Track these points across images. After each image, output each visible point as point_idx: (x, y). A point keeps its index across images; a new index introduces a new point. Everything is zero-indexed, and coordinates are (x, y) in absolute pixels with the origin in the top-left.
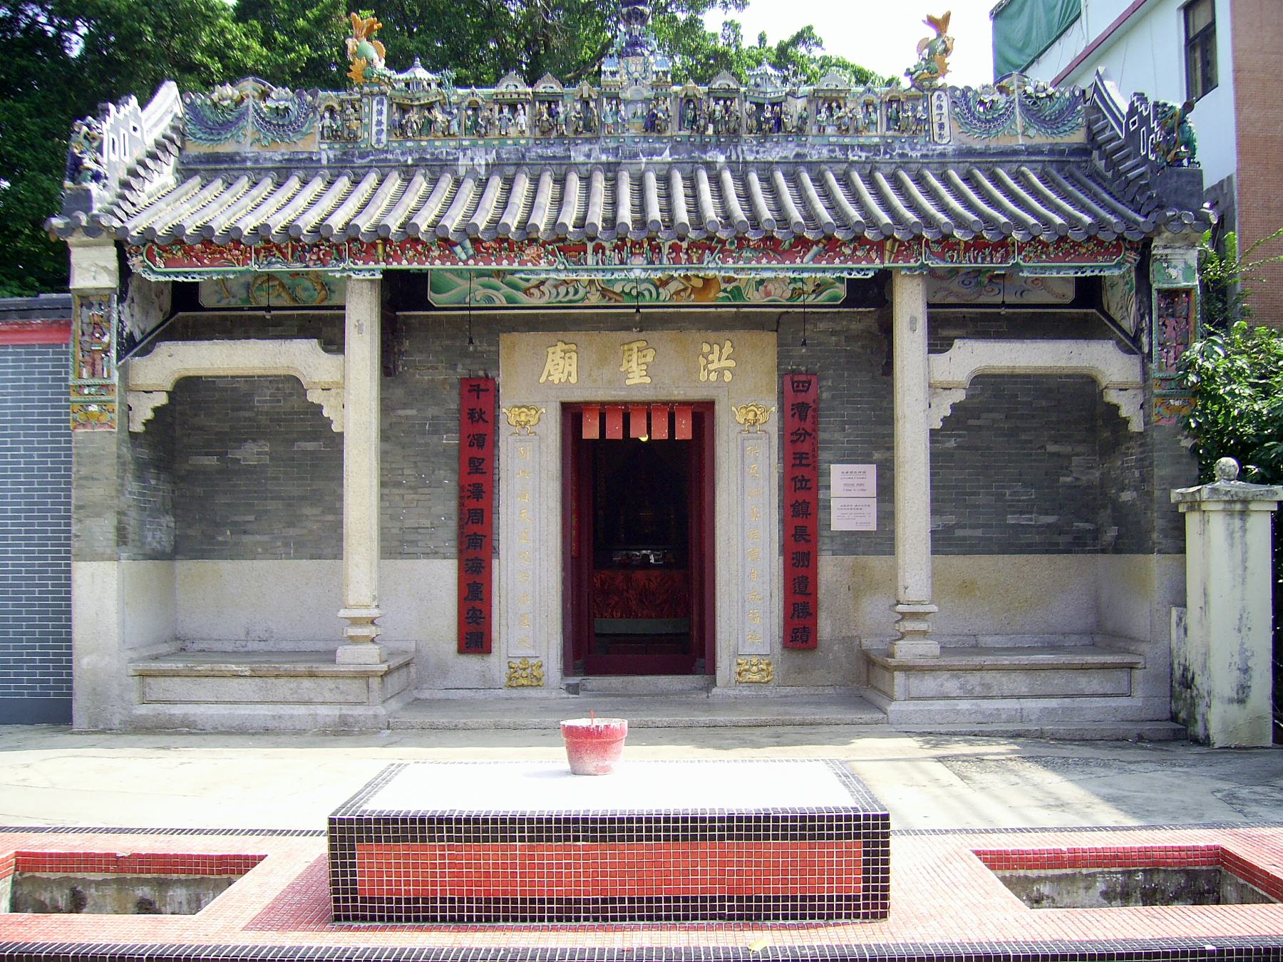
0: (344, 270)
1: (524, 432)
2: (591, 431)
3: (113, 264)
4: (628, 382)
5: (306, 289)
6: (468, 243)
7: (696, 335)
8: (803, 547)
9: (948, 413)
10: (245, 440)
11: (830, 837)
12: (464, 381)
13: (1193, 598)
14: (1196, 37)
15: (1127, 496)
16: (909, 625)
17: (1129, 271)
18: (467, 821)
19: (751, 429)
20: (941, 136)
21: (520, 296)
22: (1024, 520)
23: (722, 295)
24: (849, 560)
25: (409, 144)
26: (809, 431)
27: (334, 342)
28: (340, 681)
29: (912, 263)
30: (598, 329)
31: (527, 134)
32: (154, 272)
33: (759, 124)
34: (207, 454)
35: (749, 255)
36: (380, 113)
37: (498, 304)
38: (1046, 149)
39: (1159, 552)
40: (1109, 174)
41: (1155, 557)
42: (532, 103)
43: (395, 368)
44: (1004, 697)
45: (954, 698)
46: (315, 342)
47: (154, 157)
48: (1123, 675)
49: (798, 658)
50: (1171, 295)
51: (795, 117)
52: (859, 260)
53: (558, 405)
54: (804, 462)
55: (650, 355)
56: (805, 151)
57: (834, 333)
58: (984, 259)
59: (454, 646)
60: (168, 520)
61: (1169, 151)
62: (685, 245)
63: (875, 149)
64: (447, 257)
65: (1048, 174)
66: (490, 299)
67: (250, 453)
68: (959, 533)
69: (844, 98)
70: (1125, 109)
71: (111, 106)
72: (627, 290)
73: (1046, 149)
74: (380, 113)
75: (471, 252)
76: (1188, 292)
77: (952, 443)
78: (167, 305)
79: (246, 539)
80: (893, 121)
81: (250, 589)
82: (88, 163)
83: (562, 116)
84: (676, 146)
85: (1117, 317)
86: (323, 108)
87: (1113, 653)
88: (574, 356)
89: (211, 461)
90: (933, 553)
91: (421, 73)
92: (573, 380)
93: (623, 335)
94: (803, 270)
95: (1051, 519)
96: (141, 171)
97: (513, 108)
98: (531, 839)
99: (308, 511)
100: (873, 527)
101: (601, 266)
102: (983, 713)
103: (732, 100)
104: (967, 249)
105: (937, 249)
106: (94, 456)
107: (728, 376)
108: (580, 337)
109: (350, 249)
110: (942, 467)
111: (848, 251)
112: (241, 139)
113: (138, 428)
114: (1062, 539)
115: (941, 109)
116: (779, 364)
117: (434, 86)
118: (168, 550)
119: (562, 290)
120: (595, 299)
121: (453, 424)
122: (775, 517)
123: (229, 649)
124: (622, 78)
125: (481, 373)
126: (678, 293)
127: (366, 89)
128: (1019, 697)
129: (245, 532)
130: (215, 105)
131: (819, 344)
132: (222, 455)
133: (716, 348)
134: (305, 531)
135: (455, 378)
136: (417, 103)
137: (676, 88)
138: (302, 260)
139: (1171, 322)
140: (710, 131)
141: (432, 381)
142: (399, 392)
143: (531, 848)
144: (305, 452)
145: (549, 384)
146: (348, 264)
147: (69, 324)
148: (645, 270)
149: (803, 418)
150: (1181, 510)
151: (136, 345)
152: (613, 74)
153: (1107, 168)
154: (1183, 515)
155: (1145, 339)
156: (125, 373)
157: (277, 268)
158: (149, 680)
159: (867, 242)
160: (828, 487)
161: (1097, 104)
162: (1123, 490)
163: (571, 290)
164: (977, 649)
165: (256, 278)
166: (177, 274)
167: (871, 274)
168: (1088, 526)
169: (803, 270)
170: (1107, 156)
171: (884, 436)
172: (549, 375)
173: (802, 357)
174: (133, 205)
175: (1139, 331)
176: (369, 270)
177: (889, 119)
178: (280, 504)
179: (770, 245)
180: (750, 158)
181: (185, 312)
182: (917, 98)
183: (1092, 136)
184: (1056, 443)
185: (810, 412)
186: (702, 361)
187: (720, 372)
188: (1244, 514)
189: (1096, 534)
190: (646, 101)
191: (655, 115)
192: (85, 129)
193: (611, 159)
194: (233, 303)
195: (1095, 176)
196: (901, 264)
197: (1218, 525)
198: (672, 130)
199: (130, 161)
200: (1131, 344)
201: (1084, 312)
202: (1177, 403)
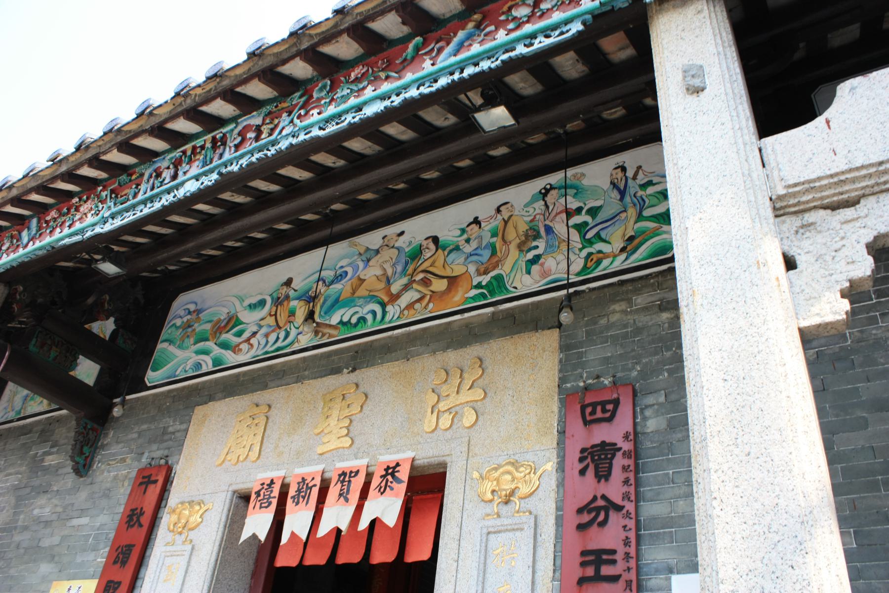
37: (205, 369)
54: (606, 570)
72: (345, 319)
116: (562, 381)
126: (410, 306)
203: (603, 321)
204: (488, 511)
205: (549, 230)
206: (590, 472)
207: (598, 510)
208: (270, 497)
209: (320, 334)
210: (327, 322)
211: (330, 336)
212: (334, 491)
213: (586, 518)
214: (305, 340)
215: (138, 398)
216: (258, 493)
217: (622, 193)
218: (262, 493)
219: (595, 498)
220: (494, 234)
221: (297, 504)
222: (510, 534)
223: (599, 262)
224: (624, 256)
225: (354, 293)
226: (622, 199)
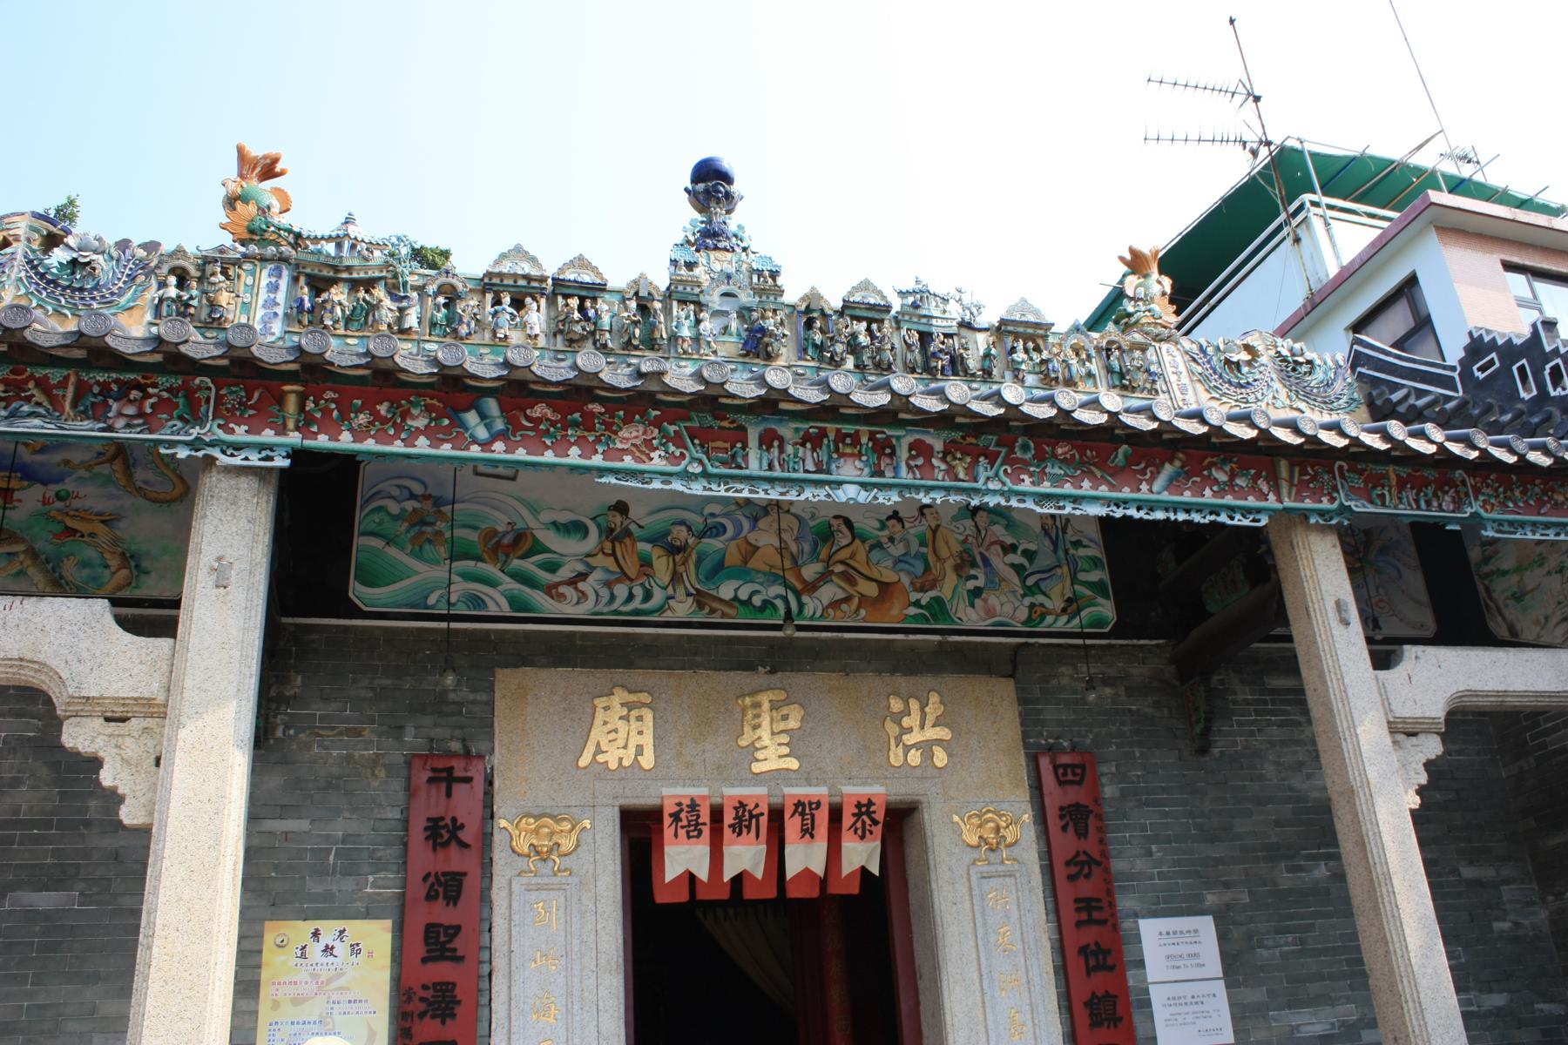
0: (195, 445)
1: (546, 869)
2: (682, 858)
5: (84, 564)
7: (868, 683)
9: (1423, 779)
19: (992, 856)
21: (539, 598)
26: (1097, 856)
27: (152, 615)
29: (1325, 504)
30: (692, 666)
31: (542, 342)
35: (1057, 471)
36: (274, 288)
37: (493, 610)
53: (617, 810)
54: (1095, 915)
66: (477, 601)
69: (1045, 337)
72: (743, 595)
74: (274, 288)
75: (499, 425)
86: (165, 269)
88: (648, 715)
92: (647, 761)
93: (741, 678)
101: (778, 473)
107: (940, 758)
108: (657, 677)
109: (219, 398)
116: (1025, 735)
119: (621, 591)
125: (456, 746)
126: (835, 604)
133: (914, 705)
135: (397, 757)
136: (345, 275)
138: (97, 412)
140: (850, 363)
141: (349, 758)
145: (600, 771)
148: (864, 485)
149: (1082, 833)
157: (34, 425)
160: (1141, 964)
172: (598, 751)
176: (261, 447)
184: (1471, 863)
185: (1091, 820)
187: (926, 747)
191: (763, 330)
203: (1054, 682)
204: (976, 856)
205: (986, 561)
206: (1070, 829)
207: (1082, 863)
208: (697, 824)
209: (707, 610)
210: (714, 593)
211: (724, 615)
212: (792, 826)
213: (1073, 870)
214: (682, 609)
215: (346, 628)
216: (676, 817)
217: (1055, 544)
218: (683, 815)
219: (1078, 854)
220: (923, 544)
221: (740, 834)
222: (1000, 880)
223: (1043, 617)
224: (1065, 618)
225: (745, 561)
226: (1055, 551)
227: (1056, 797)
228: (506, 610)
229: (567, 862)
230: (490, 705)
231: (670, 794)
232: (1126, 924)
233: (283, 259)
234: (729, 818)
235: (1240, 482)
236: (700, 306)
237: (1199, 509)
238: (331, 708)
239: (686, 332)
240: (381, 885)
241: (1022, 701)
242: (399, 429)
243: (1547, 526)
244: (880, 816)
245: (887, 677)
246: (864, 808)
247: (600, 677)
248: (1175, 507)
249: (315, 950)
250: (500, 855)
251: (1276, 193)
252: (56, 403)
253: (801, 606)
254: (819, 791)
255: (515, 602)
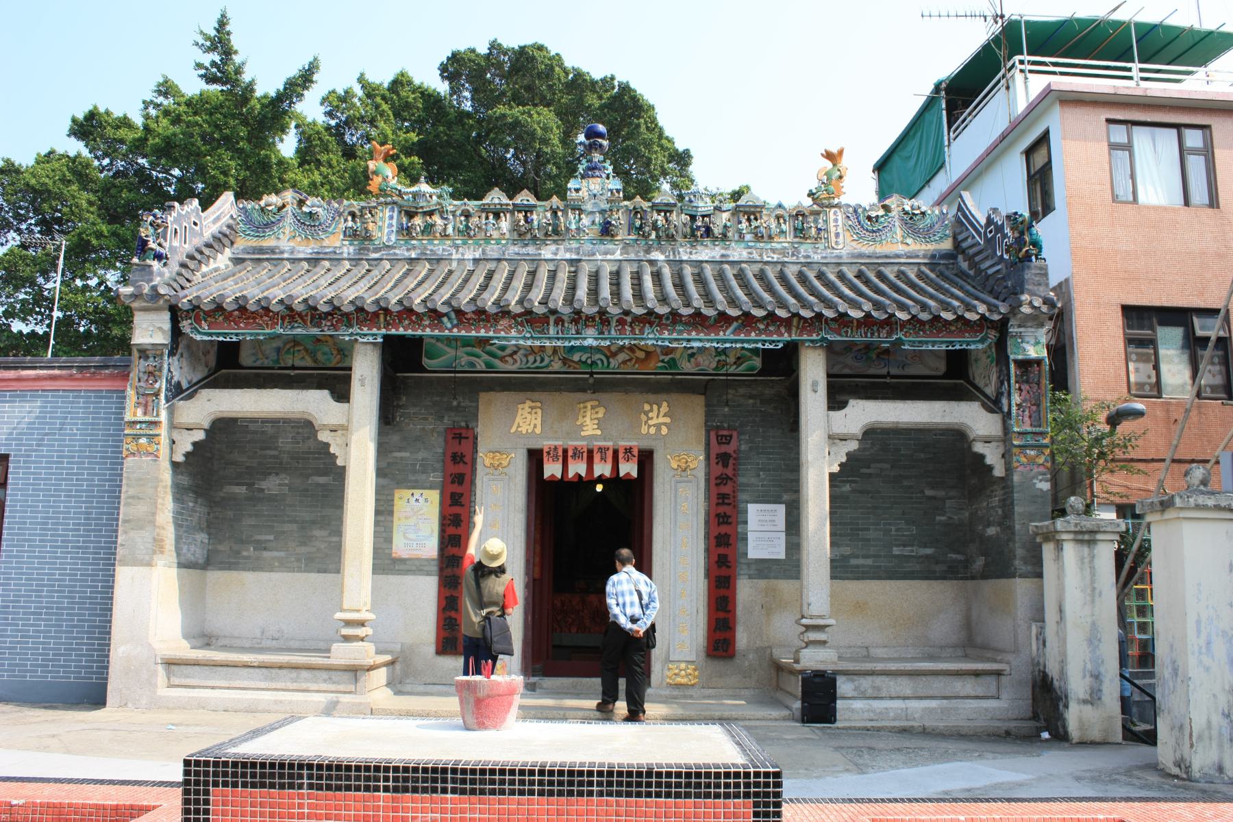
1: (497, 473)
2: (552, 469)
3: (167, 326)
4: (583, 434)
5: (324, 354)
6: (453, 315)
7: (636, 397)
8: (724, 572)
9: (844, 460)
10: (270, 474)
11: (717, 796)
12: (448, 430)
13: (1051, 615)
14: (1036, 173)
15: (992, 531)
16: (813, 636)
17: (990, 346)
18: (329, 767)
20: (837, 243)
21: (497, 362)
22: (907, 551)
23: (660, 364)
24: (762, 583)
25: (414, 242)
27: (342, 394)
28: (333, 673)
29: (814, 337)
30: (559, 390)
32: (200, 333)
33: (693, 230)
34: (238, 484)
37: (479, 368)
38: (921, 254)
39: (1021, 576)
40: (972, 272)
41: (1018, 580)
42: (512, 213)
43: (394, 418)
44: (892, 698)
45: (849, 698)
46: (326, 392)
47: (208, 246)
48: (992, 680)
49: (719, 665)
50: (1026, 365)
51: (721, 227)
52: (771, 334)
53: (525, 452)
55: (601, 411)
56: (728, 252)
57: (751, 397)
58: (872, 334)
59: (432, 649)
60: (202, 537)
61: (1020, 250)
62: (629, 319)
63: (783, 252)
64: (436, 325)
65: (923, 273)
66: (472, 364)
67: (272, 485)
68: (854, 562)
70: (983, 221)
71: (176, 204)
72: (584, 359)
73: (921, 254)
74: (391, 218)
75: (455, 322)
76: (1039, 362)
77: (847, 488)
78: (213, 363)
79: (266, 554)
80: (800, 232)
81: (263, 596)
82: (152, 245)
83: (536, 223)
84: (626, 247)
85: (981, 385)
87: (988, 660)
88: (539, 411)
89: (242, 490)
90: (832, 578)
91: (424, 187)
92: (538, 431)
93: (580, 395)
94: (725, 341)
95: (929, 551)
96: (198, 256)
97: (497, 216)
98: (396, 790)
99: (317, 533)
100: (782, 556)
102: (873, 711)
103: (671, 212)
104: (859, 327)
105: (834, 325)
106: (141, 479)
107: (664, 430)
108: (544, 396)
110: (839, 507)
111: (762, 326)
112: (281, 236)
113: (179, 458)
114: (939, 568)
115: (835, 220)
116: (706, 421)
117: (434, 198)
118: (201, 561)
119: (531, 358)
120: (557, 366)
121: (439, 465)
122: (702, 546)
123: (247, 645)
124: (584, 193)
125: (463, 424)
126: (624, 362)
127: (382, 199)
128: (905, 698)
129: (265, 549)
130: (262, 209)
131: (739, 406)
132: (250, 486)
133: (655, 407)
134: (313, 550)
135: (441, 428)
137: (626, 203)
138: (318, 325)
139: (1025, 387)
140: (653, 236)
141: (423, 429)
142: (395, 438)
143: (394, 800)
144: (318, 485)
145: (518, 434)
146: (355, 329)
147: (128, 375)
148: (596, 339)
149: (725, 465)
150: (1038, 540)
151: (182, 391)
152: (577, 190)
153: (970, 267)
154: (1040, 546)
155: (1005, 401)
156: (171, 411)
157: (299, 331)
158: (173, 667)
159: (780, 319)
160: (746, 523)
161: (963, 220)
162: (989, 526)
163: (538, 359)
164: (868, 658)
165: (285, 344)
166: (218, 335)
167: (781, 345)
168: (960, 557)
169: (725, 341)
170: (970, 259)
171: (792, 481)
173: (725, 416)
174: (188, 280)
175: (999, 394)
177: (796, 229)
178: (295, 526)
179: (698, 320)
180: (685, 258)
181: (226, 366)
182: (817, 213)
183: (957, 244)
184: (933, 488)
185: (731, 461)
186: (644, 418)
187: (658, 426)
188: (1091, 543)
189: (967, 563)
190: (602, 212)
191: (609, 223)
192: (151, 218)
193: (574, 257)
194: (266, 363)
195: (962, 274)
196: (805, 337)
197: (1070, 550)
198: (622, 234)
199: (188, 248)
200: (993, 405)
201: (954, 379)
202: (1032, 453)
212: (597, 457)
216: (548, 453)
227: (716, 449)
228: (484, 368)
229: (505, 470)
230: (477, 408)
231: (546, 444)
232: (742, 505)
233: (394, 203)
234: (570, 453)
235: (771, 328)
236: (581, 211)
237: (748, 341)
238: (416, 409)
239: (573, 227)
240: (436, 477)
241: (707, 405)
242: (420, 325)
243: (942, 342)
244: (636, 452)
245: (645, 395)
246: (628, 450)
247: (521, 395)
248: (736, 341)
249: (413, 500)
250: (479, 467)
251: (1001, 54)
252: (305, 322)
253: (609, 363)
254: (610, 444)
255: (488, 365)
